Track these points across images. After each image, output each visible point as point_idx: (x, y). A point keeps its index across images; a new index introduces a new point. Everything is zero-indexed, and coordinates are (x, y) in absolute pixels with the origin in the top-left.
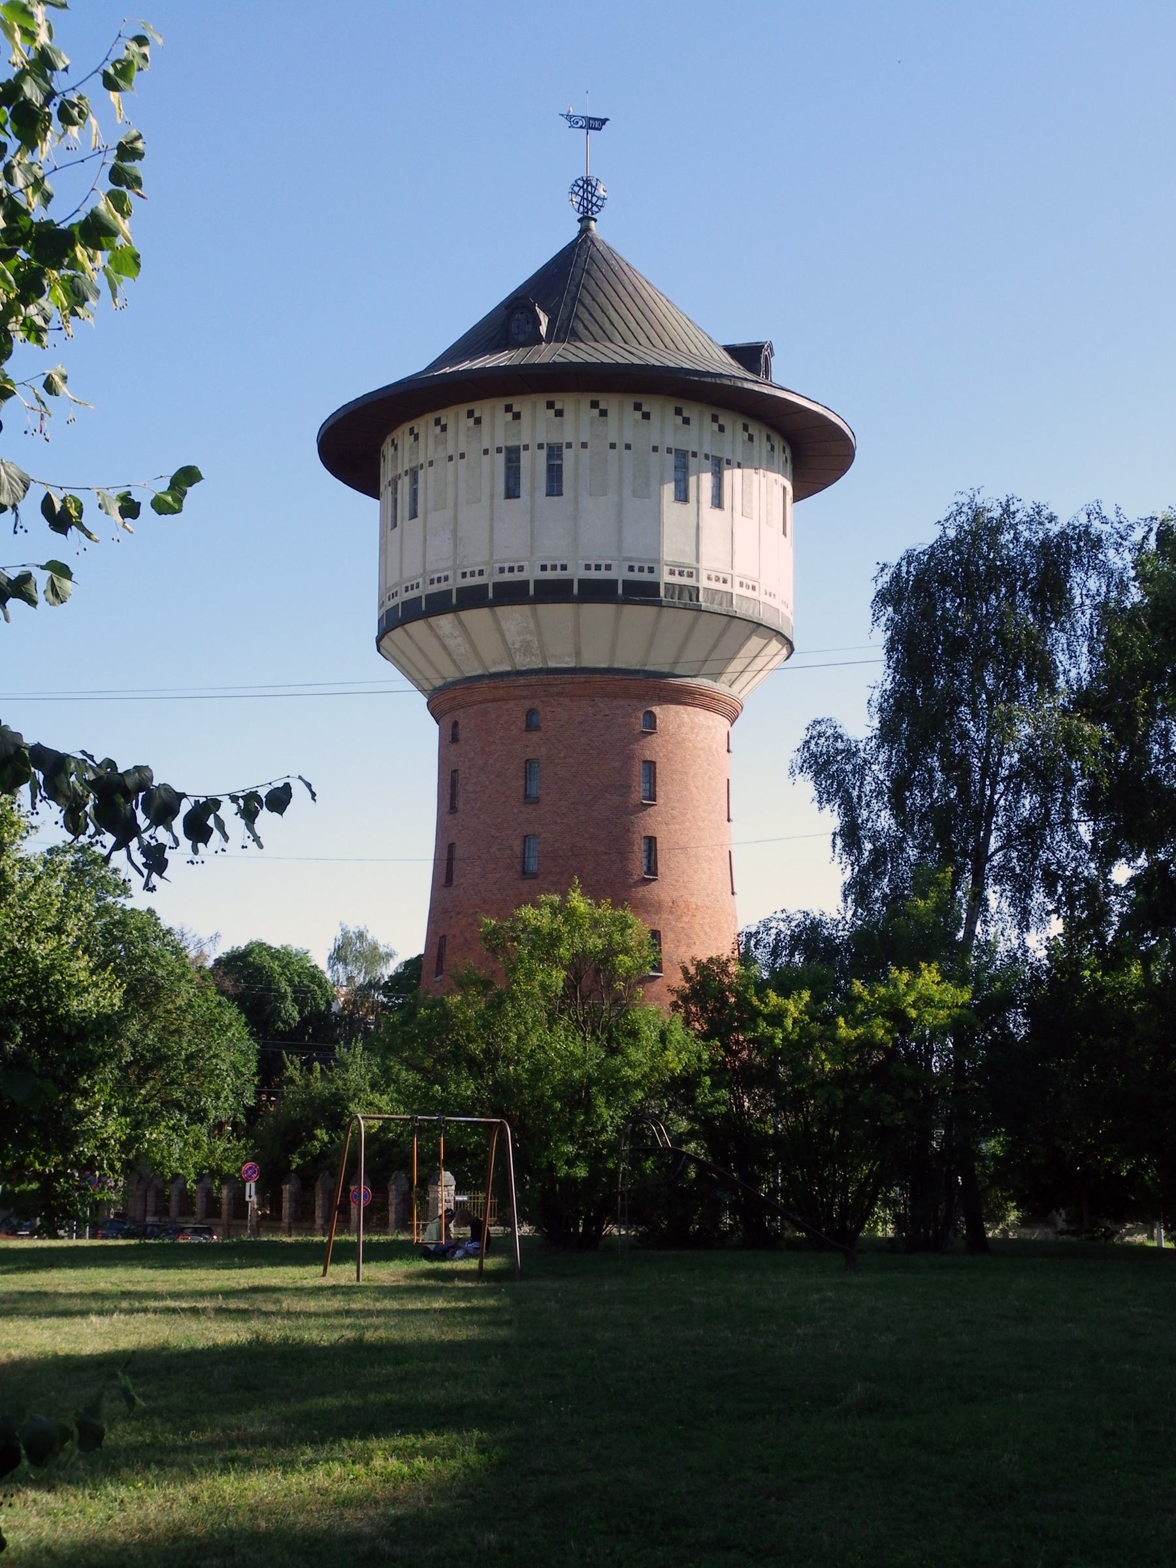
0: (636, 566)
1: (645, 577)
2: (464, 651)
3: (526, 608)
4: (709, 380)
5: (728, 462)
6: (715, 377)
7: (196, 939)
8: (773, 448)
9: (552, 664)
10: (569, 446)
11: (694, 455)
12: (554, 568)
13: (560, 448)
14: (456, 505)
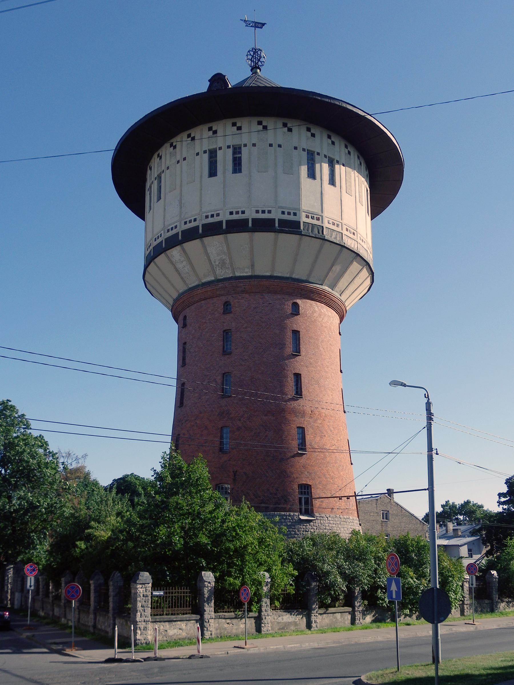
0: (286, 211)
1: (292, 218)
2: (187, 271)
3: (221, 237)
4: (327, 100)
5: (338, 162)
6: (331, 100)
7: (75, 456)
8: (361, 164)
9: (238, 274)
10: (245, 145)
11: (318, 154)
12: (237, 213)
13: (240, 148)
14: (181, 186)
